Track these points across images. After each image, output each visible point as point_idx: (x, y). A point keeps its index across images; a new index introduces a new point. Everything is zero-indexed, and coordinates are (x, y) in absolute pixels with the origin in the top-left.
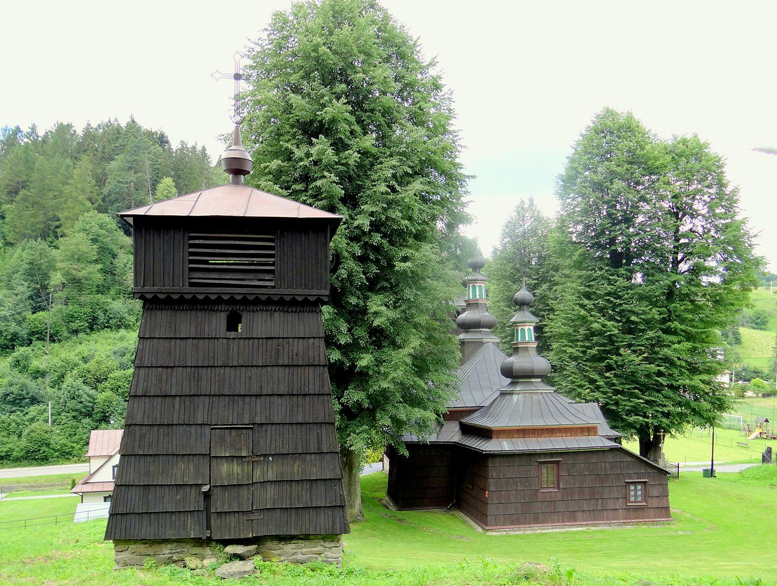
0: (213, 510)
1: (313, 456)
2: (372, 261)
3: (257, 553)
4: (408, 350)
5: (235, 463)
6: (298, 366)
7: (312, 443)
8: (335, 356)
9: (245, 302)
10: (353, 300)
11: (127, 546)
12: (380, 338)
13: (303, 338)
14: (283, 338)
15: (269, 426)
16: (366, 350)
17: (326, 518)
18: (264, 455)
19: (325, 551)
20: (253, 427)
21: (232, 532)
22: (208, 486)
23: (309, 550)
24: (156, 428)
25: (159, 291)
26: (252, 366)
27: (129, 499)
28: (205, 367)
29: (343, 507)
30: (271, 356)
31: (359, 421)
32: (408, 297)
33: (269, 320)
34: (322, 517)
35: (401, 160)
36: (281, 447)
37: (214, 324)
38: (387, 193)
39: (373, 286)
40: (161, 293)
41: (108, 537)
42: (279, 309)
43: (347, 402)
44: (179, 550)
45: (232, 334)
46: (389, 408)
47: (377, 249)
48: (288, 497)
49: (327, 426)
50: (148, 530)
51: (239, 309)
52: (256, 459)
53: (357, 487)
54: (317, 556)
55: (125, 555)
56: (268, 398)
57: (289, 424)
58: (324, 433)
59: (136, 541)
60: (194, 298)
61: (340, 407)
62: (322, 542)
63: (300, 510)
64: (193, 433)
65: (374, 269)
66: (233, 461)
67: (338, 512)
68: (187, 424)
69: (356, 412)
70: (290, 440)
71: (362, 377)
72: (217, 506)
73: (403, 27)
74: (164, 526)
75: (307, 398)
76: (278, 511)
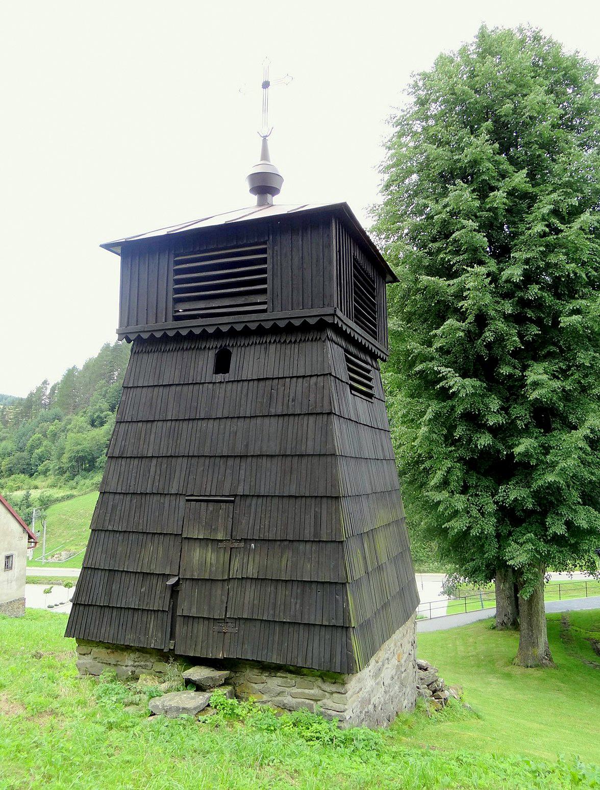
0: (179, 613)
1: (308, 546)
2: (531, 320)
3: (227, 683)
4: (583, 431)
5: (210, 550)
6: (294, 415)
7: (307, 526)
8: (484, 440)
9: (232, 333)
10: (505, 370)
11: (90, 648)
12: (546, 417)
13: (304, 377)
14: (279, 378)
15: (255, 500)
16: (526, 432)
17: (322, 643)
18: (245, 540)
19: (324, 696)
20: (234, 499)
21: (199, 647)
22: (177, 579)
23: (300, 690)
24: (129, 497)
25: (142, 330)
26: (238, 417)
27: (93, 586)
28: (187, 419)
29: (347, 628)
30: (262, 403)
31: (526, 529)
32: (582, 361)
33: (262, 356)
34: (316, 641)
35: (566, 194)
36: (266, 529)
37: (200, 363)
38: (545, 235)
39: (531, 352)
40: (144, 332)
41: (68, 634)
42: (275, 341)
43: (502, 501)
44: (142, 663)
45: (219, 377)
46: (563, 510)
47: (538, 304)
48: (271, 605)
49: (330, 501)
50: (108, 632)
51: (229, 345)
52: (236, 545)
53: (540, 618)
54: (312, 702)
55: (88, 660)
56: (254, 460)
57: (279, 496)
58: (324, 513)
59: (100, 643)
60: (178, 334)
61: (495, 507)
62: (320, 681)
63: (286, 626)
64: (166, 505)
65: (535, 330)
66: (207, 546)
67: (339, 633)
68: (161, 494)
69: (521, 516)
70: (279, 520)
71: (520, 469)
72: (184, 608)
73: (578, 53)
74: (124, 627)
75: (305, 460)
76: (258, 623)
